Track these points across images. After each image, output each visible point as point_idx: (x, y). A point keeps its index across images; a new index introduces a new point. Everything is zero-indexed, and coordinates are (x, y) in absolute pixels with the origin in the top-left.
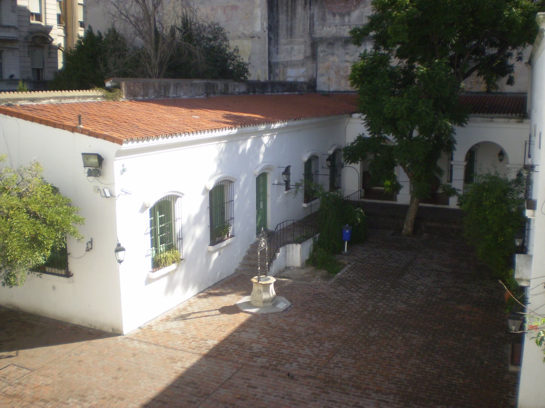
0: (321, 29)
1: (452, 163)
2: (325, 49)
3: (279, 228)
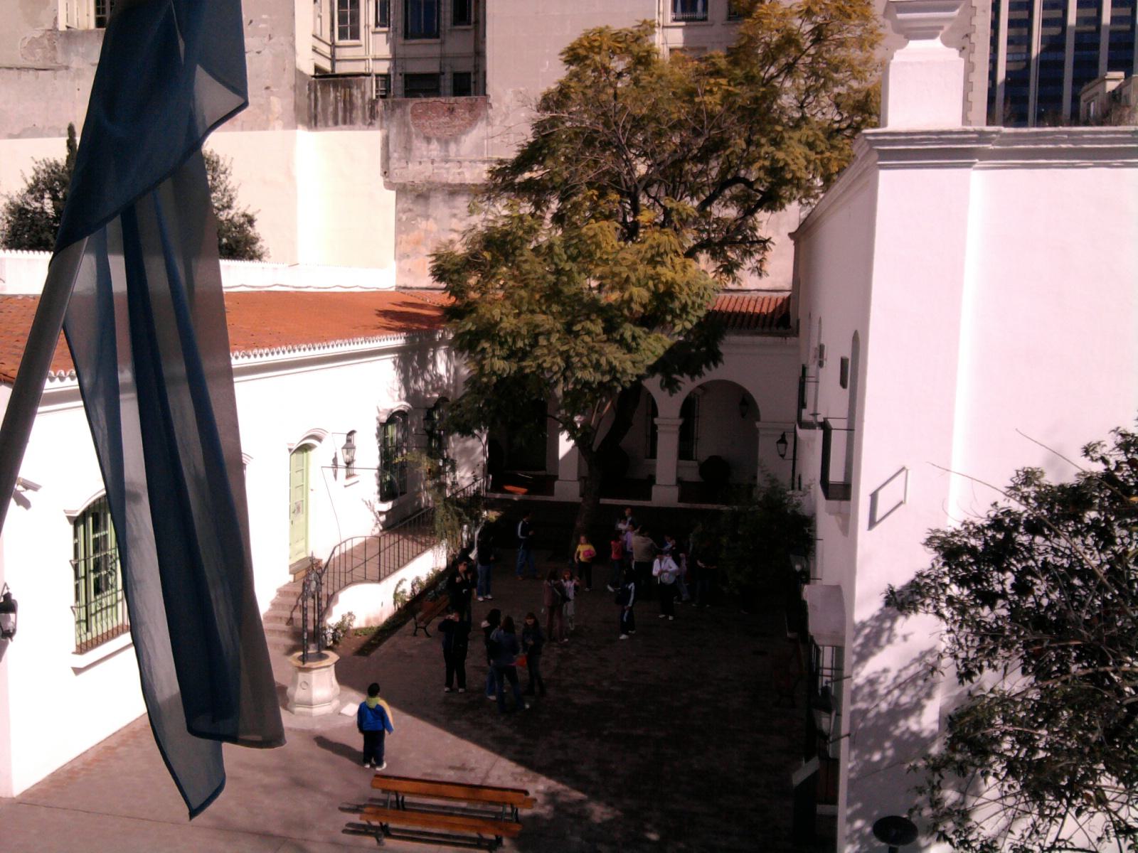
0: (403, 168)
1: (656, 421)
2: (411, 206)
3: (337, 553)
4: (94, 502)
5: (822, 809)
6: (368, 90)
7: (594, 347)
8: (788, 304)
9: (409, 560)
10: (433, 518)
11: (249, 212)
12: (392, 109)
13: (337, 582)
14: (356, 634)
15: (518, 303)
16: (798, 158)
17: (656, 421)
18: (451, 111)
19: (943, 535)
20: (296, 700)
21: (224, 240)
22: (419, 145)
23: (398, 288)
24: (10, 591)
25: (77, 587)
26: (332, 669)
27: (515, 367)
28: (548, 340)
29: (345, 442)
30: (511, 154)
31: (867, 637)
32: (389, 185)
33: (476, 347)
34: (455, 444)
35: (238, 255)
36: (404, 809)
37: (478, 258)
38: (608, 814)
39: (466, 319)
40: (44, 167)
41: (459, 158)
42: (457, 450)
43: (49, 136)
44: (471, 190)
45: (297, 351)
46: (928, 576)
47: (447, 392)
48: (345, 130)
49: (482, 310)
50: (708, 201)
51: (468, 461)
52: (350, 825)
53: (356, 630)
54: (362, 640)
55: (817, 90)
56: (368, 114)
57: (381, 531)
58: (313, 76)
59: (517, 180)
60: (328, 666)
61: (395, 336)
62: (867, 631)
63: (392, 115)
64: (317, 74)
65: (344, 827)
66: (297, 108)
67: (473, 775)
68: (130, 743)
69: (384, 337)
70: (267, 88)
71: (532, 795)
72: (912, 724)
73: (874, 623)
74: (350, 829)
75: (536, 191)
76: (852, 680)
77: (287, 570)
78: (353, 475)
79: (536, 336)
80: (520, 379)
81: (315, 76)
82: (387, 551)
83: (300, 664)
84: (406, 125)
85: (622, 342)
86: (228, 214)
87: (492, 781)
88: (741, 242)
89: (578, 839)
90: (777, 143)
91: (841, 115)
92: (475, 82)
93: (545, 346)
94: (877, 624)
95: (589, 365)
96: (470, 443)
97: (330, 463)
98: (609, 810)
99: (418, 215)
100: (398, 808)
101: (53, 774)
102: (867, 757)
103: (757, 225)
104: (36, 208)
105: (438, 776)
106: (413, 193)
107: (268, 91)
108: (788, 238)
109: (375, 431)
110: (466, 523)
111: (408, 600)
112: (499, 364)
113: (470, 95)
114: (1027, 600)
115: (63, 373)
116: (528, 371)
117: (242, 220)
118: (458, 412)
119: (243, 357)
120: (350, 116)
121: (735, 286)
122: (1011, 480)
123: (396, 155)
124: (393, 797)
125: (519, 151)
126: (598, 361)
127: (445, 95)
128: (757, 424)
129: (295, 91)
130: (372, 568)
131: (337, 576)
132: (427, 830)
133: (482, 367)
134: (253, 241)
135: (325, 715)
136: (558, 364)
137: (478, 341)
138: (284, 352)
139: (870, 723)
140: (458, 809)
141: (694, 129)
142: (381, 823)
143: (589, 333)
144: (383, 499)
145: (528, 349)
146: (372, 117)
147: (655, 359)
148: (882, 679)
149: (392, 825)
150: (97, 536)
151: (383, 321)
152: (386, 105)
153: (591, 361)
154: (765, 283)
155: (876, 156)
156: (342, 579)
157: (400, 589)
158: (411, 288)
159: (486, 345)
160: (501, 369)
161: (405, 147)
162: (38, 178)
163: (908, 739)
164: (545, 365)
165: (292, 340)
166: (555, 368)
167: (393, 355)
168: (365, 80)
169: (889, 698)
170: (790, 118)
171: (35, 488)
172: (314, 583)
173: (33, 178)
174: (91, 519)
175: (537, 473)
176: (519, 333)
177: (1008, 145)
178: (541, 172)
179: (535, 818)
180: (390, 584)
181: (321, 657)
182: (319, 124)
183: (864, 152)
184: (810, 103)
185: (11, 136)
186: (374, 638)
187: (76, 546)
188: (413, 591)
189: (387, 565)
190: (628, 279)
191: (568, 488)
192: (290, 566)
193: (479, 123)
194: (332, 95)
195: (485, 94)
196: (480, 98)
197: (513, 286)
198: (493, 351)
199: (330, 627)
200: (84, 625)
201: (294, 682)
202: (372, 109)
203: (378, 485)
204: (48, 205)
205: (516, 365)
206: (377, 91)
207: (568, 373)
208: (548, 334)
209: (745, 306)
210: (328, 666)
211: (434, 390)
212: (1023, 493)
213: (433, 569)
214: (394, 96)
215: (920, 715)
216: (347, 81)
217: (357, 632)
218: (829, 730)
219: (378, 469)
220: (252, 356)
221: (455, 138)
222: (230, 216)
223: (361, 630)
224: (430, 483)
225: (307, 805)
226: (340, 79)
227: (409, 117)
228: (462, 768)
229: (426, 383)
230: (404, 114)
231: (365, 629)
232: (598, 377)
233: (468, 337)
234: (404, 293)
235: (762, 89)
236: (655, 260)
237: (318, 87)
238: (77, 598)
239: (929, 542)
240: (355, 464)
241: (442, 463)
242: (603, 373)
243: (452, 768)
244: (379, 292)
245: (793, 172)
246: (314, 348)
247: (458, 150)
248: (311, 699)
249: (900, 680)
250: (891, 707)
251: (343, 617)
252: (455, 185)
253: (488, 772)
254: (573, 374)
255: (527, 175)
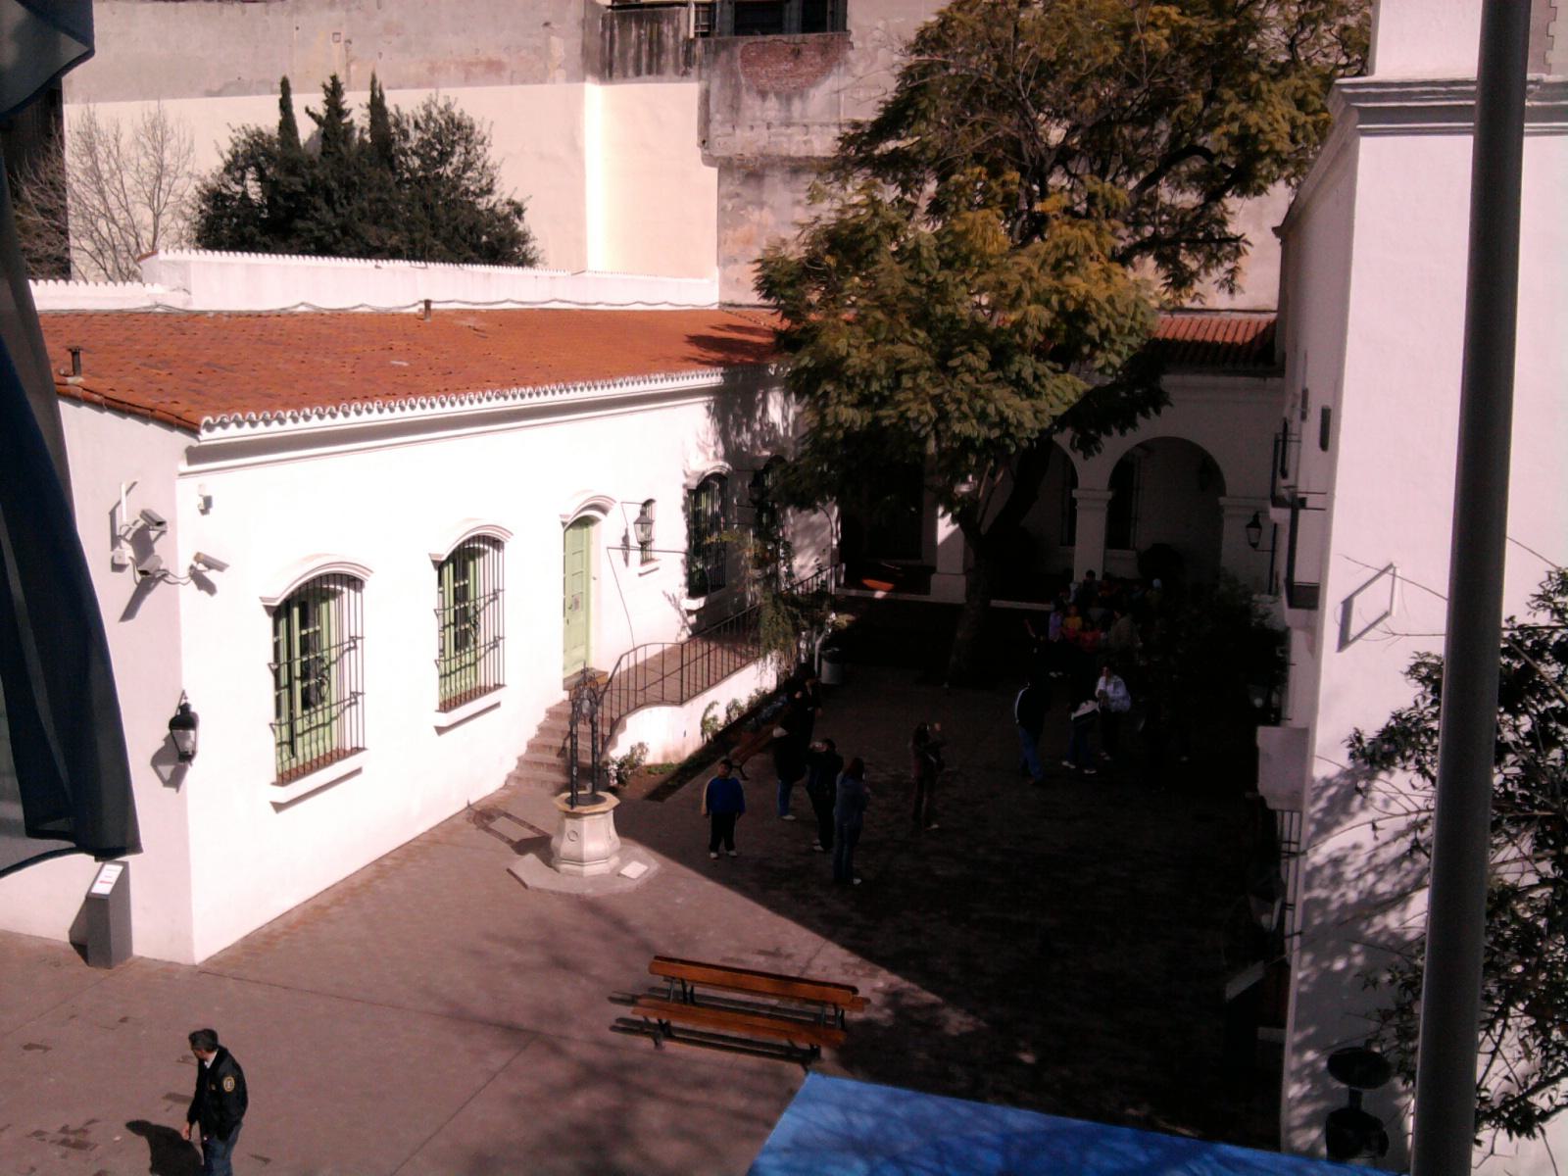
0: (729, 135)
1: (1075, 493)
3: (624, 666)
4: (299, 588)
5: (1263, 1032)
6: (683, 25)
7: (978, 390)
8: (1274, 331)
9: (724, 677)
10: (758, 621)
11: (517, 198)
12: (713, 52)
13: (624, 702)
14: (649, 772)
15: (873, 328)
16: (1278, 122)
17: (1075, 493)
18: (797, 53)
19: (1434, 661)
20: (562, 855)
21: (484, 238)
22: (750, 102)
23: (723, 305)
24: (189, 701)
25: (278, 699)
26: (611, 815)
27: (868, 417)
28: (915, 380)
29: (638, 515)
30: (869, 114)
31: (1331, 799)
32: (709, 160)
33: (817, 389)
34: (793, 520)
35: (503, 258)
36: (695, 1004)
37: (819, 265)
38: (967, 1024)
39: (801, 352)
40: (244, 137)
41: (806, 121)
42: (799, 526)
43: (258, 93)
44: (813, 166)
45: (572, 391)
46: (1408, 719)
47: (784, 450)
48: (650, 82)
49: (823, 340)
50: (1152, 180)
51: (813, 542)
52: (621, 1020)
53: (649, 767)
54: (657, 780)
55: (1315, 21)
56: (681, 59)
57: (689, 637)
58: (608, 7)
59: (877, 152)
60: (604, 812)
61: (709, 371)
62: (1332, 791)
63: (715, 61)
64: (616, 4)
65: (613, 1023)
66: (585, 51)
67: (789, 963)
68: (346, 902)
69: (693, 373)
70: (547, 24)
71: (863, 993)
72: (1392, 920)
73: (1342, 781)
74: (620, 1025)
75: (900, 167)
76: (1307, 859)
77: (560, 684)
78: (651, 560)
79: (898, 375)
80: (875, 429)
81: (611, 7)
82: (693, 665)
83: (567, 808)
84: (733, 74)
85: (1019, 385)
86: (489, 201)
87: (815, 973)
88: (1203, 241)
89: (922, 1055)
90: (1251, 97)
91: (1349, 57)
92: (832, 13)
93: (909, 389)
94: (1348, 781)
95: (971, 414)
96: (816, 518)
97: (619, 543)
98: (971, 1019)
99: (750, 203)
100: (685, 1001)
101: (246, 937)
102: (1325, 964)
103: (1228, 217)
104: (237, 193)
105: (742, 962)
106: (742, 170)
107: (547, 29)
108: (1272, 235)
109: (681, 502)
110: (805, 629)
111: (720, 729)
112: (847, 414)
113: (825, 30)
114: (1547, 755)
115: (254, 416)
116: (886, 423)
117: (507, 209)
118: (793, 477)
119: (497, 398)
120: (658, 63)
121: (1197, 305)
122: (1540, 585)
123: (718, 117)
124: (679, 987)
125: (880, 110)
126: (984, 410)
127: (790, 32)
128: (1222, 500)
129: (584, 28)
130: (672, 686)
131: (624, 694)
132: (722, 1032)
133: (823, 417)
134: (520, 239)
135: (601, 876)
136: (927, 413)
137: (819, 383)
138: (553, 392)
139: (1333, 917)
140: (764, 1007)
141: (1128, 77)
142: (660, 1021)
143: (971, 370)
144: (693, 594)
145: (886, 393)
146: (686, 64)
147: (1065, 408)
148: (1349, 860)
149: (676, 1024)
150: (304, 632)
151: (694, 351)
152: (706, 45)
153: (972, 409)
154: (1240, 301)
155: (1356, 116)
156: (632, 698)
157: (710, 716)
158: (740, 306)
159: (830, 388)
160: (850, 420)
161: (732, 106)
162: (237, 152)
163: (1386, 941)
164: (910, 414)
165: (566, 376)
166: (924, 419)
167: (706, 398)
168: (679, 11)
169: (1361, 885)
170: (1273, 64)
171: (220, 567)
172: (587, 703)
173: (230, 152)
174: (296, 611)
175: (910, 562)
176: (873, 373)
177: (1552, 100)
178: (910, 141)
179: (868, 1024)
180: (696, 708)
181: (598, 800)
182: (615, 74)
183: (1341, 110)
184: (1305, 40)
185: (210, 94)
186: (673, 778)
187: (276, 646)
188: (729, 717)
189: (692, 681)
190: (1019, 293)
191: (949, 584)
192: (565, 680)
193: (835, 70)
194: (634, 33)
195: (845, 29)
196: (835, 35)
197: (866, 305)
198: (839, 395)
199: (613, 762)
200: (286, 747)
201: (561, 831)
202: (688, 52)
203: (686, 575)
204: (254, 190)
205: (870, 415)
206: (696, 27)
207: (942, 426)
208: (915, 371)
209: (1211, 333)
210: (604, 812)
211: (765, 446)
212: (1555, 604)
213: (757, 690)
214: (720, 34)
215: (1404, 909)
216: (654, 13)
217: (650, 769)
218: (1271, 924)
219: (686, 553)
220: (510, 397)
221: (801, 92)
222: (491, 205)
223: (656, 766)
224: (757, 573)
225: (568, 992)
226: (645, 10)
227: (739, 63)
228: (776, 954)
229: (754, 435)
230: (732, 57)
231: (662, 765)
232: (984, 431)
233: (805, 376)
234: (730, 313)
235: (1233, 22)
236: (1062, 264)
237: (616, 22)
238: (278, 714)
239: (1413, 670)
240: (655, 545)
241: (773, 550)
242: (992, 426)
243: (761, 952)
244: (697, 311)
245: (1271, 143)
246: (596, 388)
247: (804, 109)
248: (581, 854)
249: (1377, 861)
250: (1363, 896)
251: (632, 749)
252: (800, 159)
253: (809, 961)
254: (948, 428)
255: (891, 145)
